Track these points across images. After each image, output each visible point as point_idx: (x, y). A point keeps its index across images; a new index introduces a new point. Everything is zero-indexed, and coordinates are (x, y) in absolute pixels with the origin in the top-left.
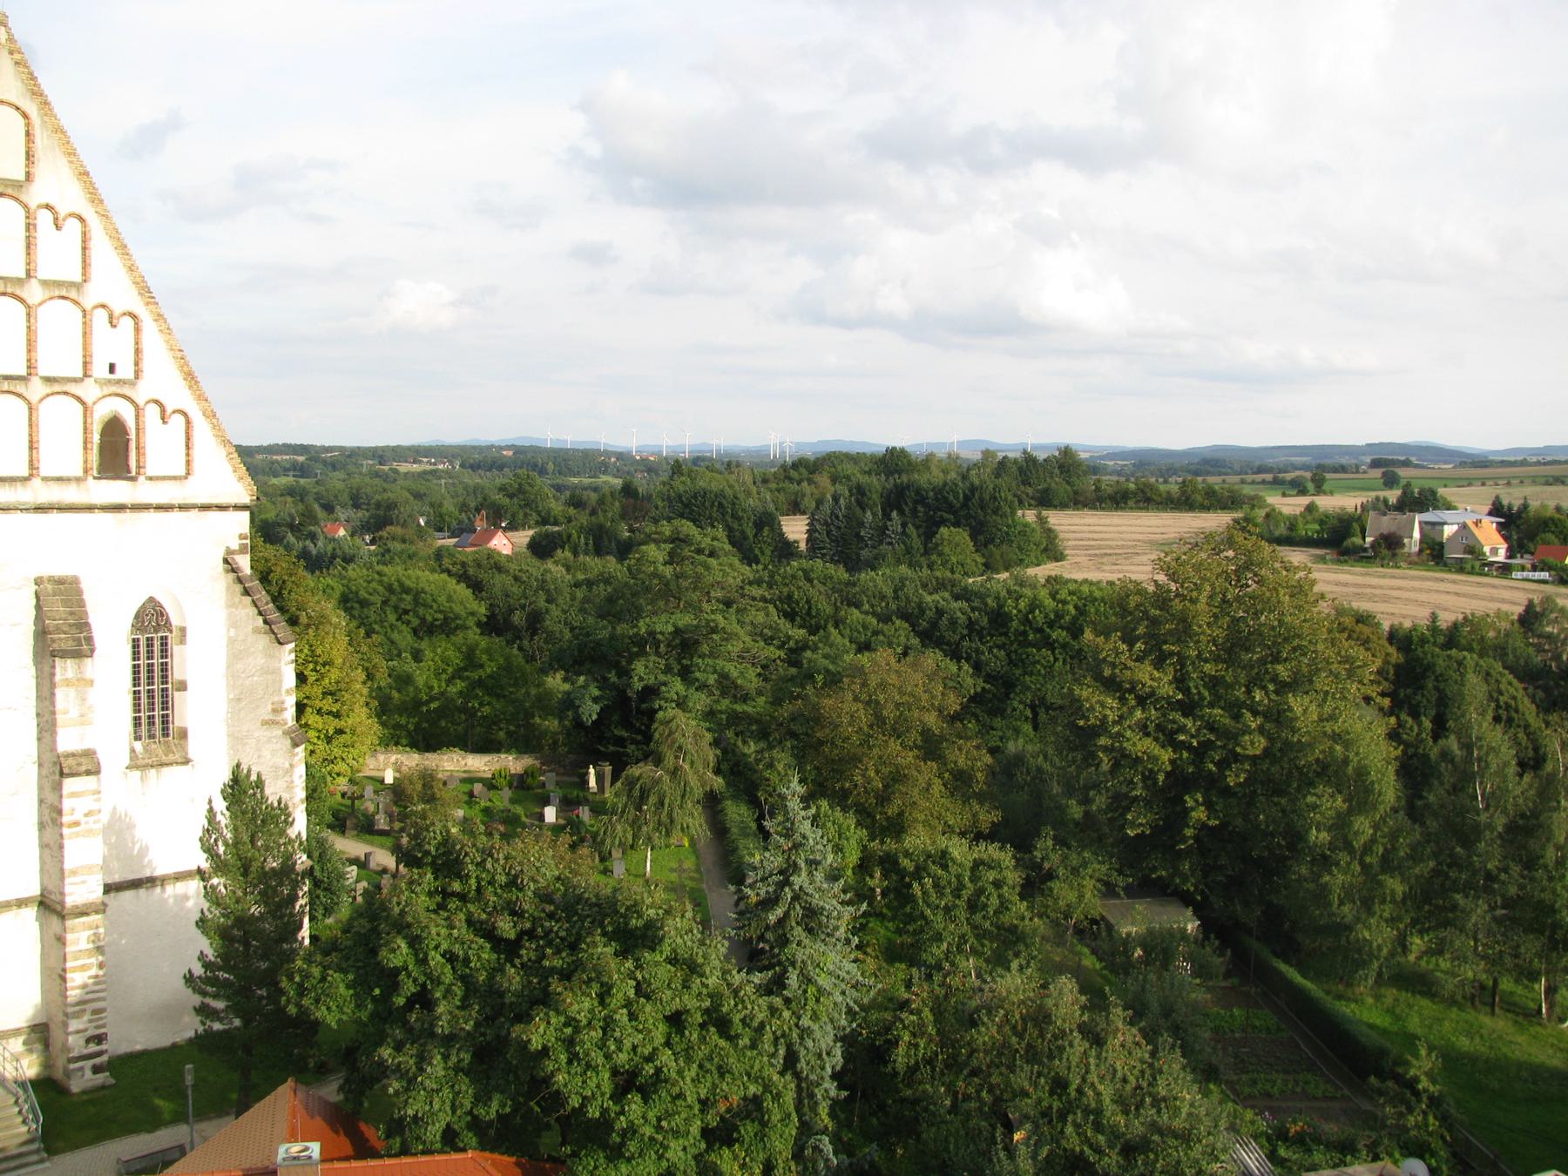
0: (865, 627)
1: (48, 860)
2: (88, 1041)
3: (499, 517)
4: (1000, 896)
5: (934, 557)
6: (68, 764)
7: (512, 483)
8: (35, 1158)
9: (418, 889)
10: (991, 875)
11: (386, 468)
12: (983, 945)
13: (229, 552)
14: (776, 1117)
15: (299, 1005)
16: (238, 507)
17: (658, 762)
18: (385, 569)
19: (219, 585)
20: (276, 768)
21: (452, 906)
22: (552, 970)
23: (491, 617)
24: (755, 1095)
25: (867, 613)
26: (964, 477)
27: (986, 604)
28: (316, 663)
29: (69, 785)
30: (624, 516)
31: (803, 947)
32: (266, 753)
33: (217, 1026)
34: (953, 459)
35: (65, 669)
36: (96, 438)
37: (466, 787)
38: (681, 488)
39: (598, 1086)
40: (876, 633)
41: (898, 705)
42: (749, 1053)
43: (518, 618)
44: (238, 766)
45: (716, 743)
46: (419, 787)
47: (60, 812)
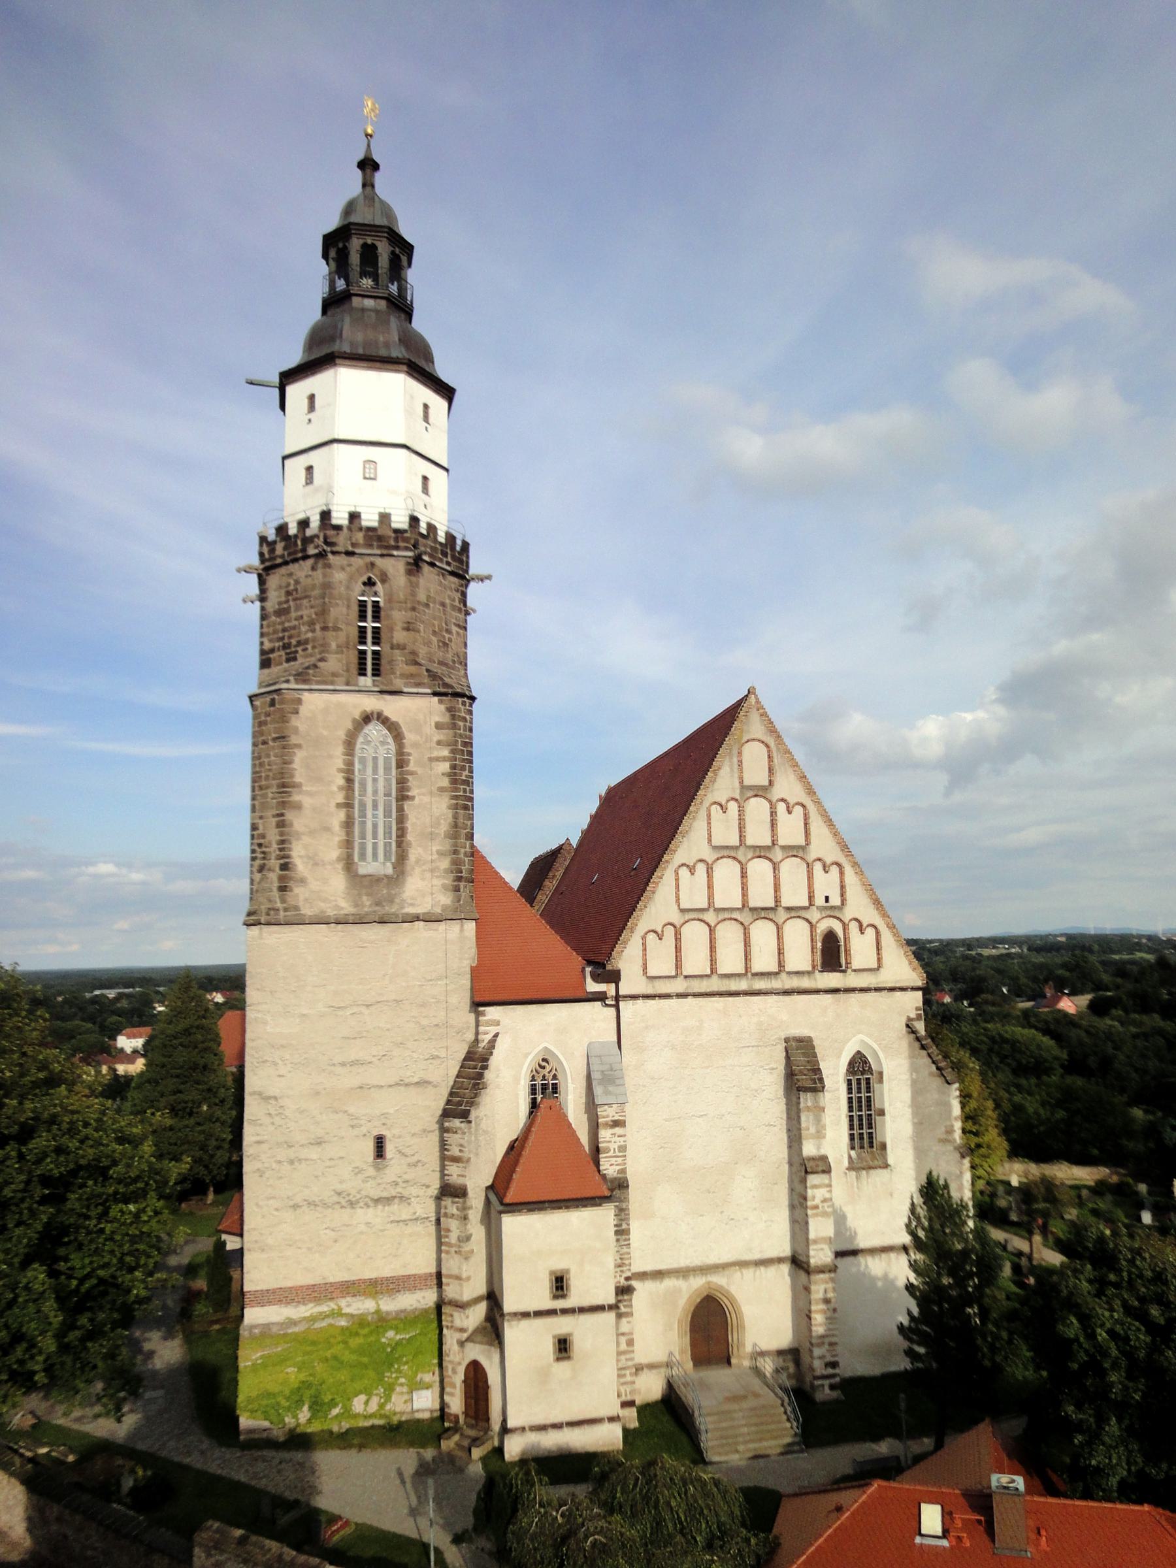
6: (809, 1165)
8: (796, 1448)
9: (1082, 1277)
11: (973, 953)
13: (909, 1019)
16: (914, 989)
19: (904, 1043)
21: (1109, 1292)
29: (812, 1179)
33: (920, 1365)
35: (806, 1100)
36: (819, 945)
43: (1092, 1062)
46: (1042, 1190)
47: (805, 1199)
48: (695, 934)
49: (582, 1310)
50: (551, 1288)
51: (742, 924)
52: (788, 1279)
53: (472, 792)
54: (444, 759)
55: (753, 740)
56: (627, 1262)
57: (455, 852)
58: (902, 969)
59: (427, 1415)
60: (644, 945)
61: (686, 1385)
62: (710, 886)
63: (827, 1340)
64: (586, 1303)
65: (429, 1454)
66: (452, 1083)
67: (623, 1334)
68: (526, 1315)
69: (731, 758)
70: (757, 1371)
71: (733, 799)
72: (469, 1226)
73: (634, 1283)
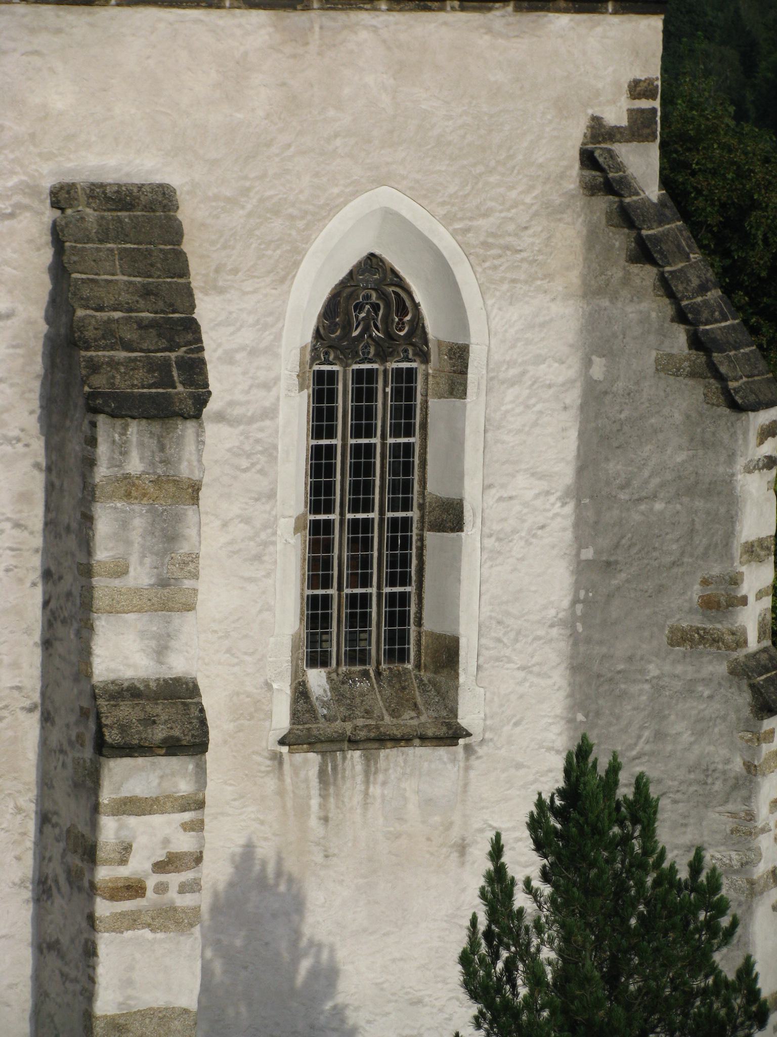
13: (599, 132)
20: (705, 771)
29: (124, 778)
32: (679, 727)
35: (124, 450)
47: (89, 852)
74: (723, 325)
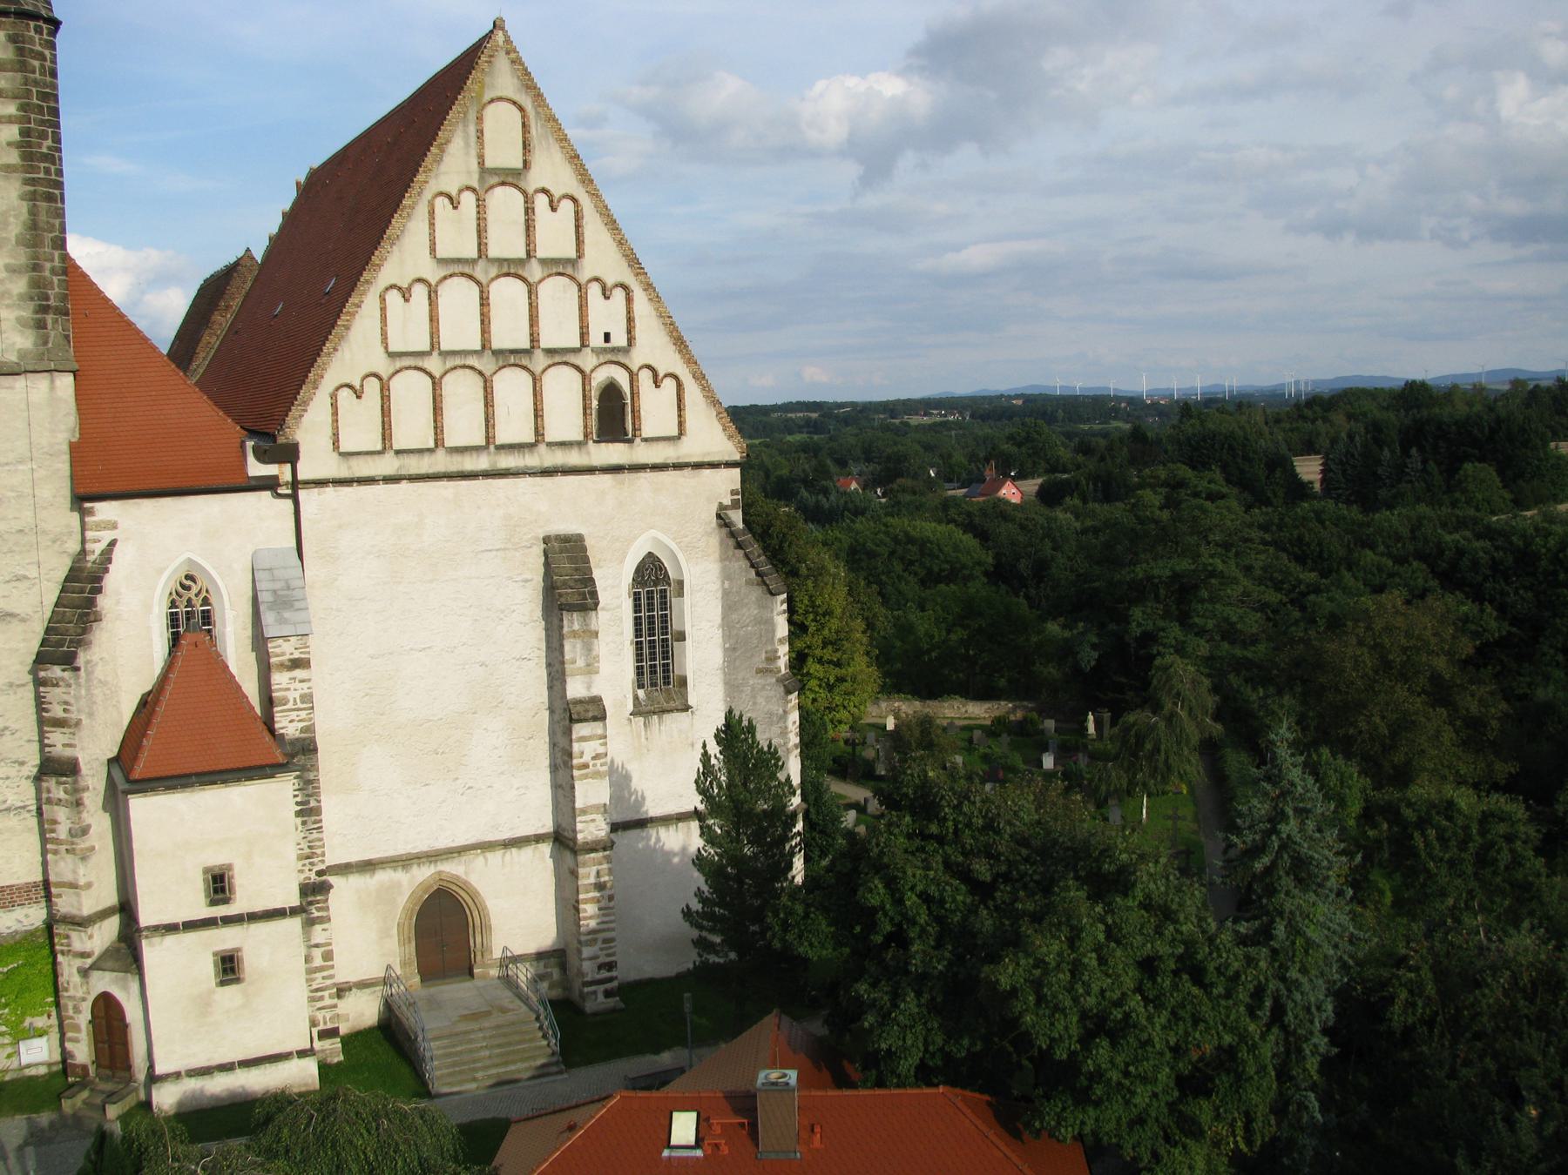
0: (1380, 569)
1: (561, 799)
2: (600, 967)
3: (1009, 467)
4: (1512, 851)
5: (1457, 495)
7: (1021, 429)
8: (554, 1069)
9: (896, 831)
10: (1502, 828)
12: (1492, 902)
13: (722, 507)
14: (1251, 1070)
15: (783, 940)
17: (1157, 708)
18: (890, 520)
20: (770, 714)
22: (1025, 913)
23: (998, 566)
24: (1230, 1046)
25: (1382, 554)
26: (1491, 409)
27: (1511, 543)
28: (817, 614)
29: (580, 730)
30: (1133, 461)
31: (1290, 898)
32: (760, 700)
33: (713, 959)
34: (1479, 390)
35: (572, 622)
36: (595, 403)
37: (966, 735)
38: (1190, 430)
39: (1066, 1028)
40: (1391, 575)
41: (1405, 650)
42: (1223, 1002)
43: (1024, 566)
44: (730, 711)
45: (1215, 689)
46: (917, 733)
47: (570, 755)
48: (411, 391)
49: (253, 917)
50: (207, 890)
51: (481, 373)
52: (550, 862)
53: (60, 173)
54: (10, 120)
55: (500, 99)
56: (319, 851)
57: (36, 268)
58: (711, 438)
59: (43, 1070)
60: (334, 406)
61: (412, 1004)
62: (434, 319)
63: (601, 936)
64: (259, 907)
65: (45, 1118)
66: (48, 614)
67: (317, 946)
68: (171, 928)
69: (466, 126)
70: (508, 982)
71: (468, 188)
72: (84, 815)
73: (332, 879)
74: (766, 568)
